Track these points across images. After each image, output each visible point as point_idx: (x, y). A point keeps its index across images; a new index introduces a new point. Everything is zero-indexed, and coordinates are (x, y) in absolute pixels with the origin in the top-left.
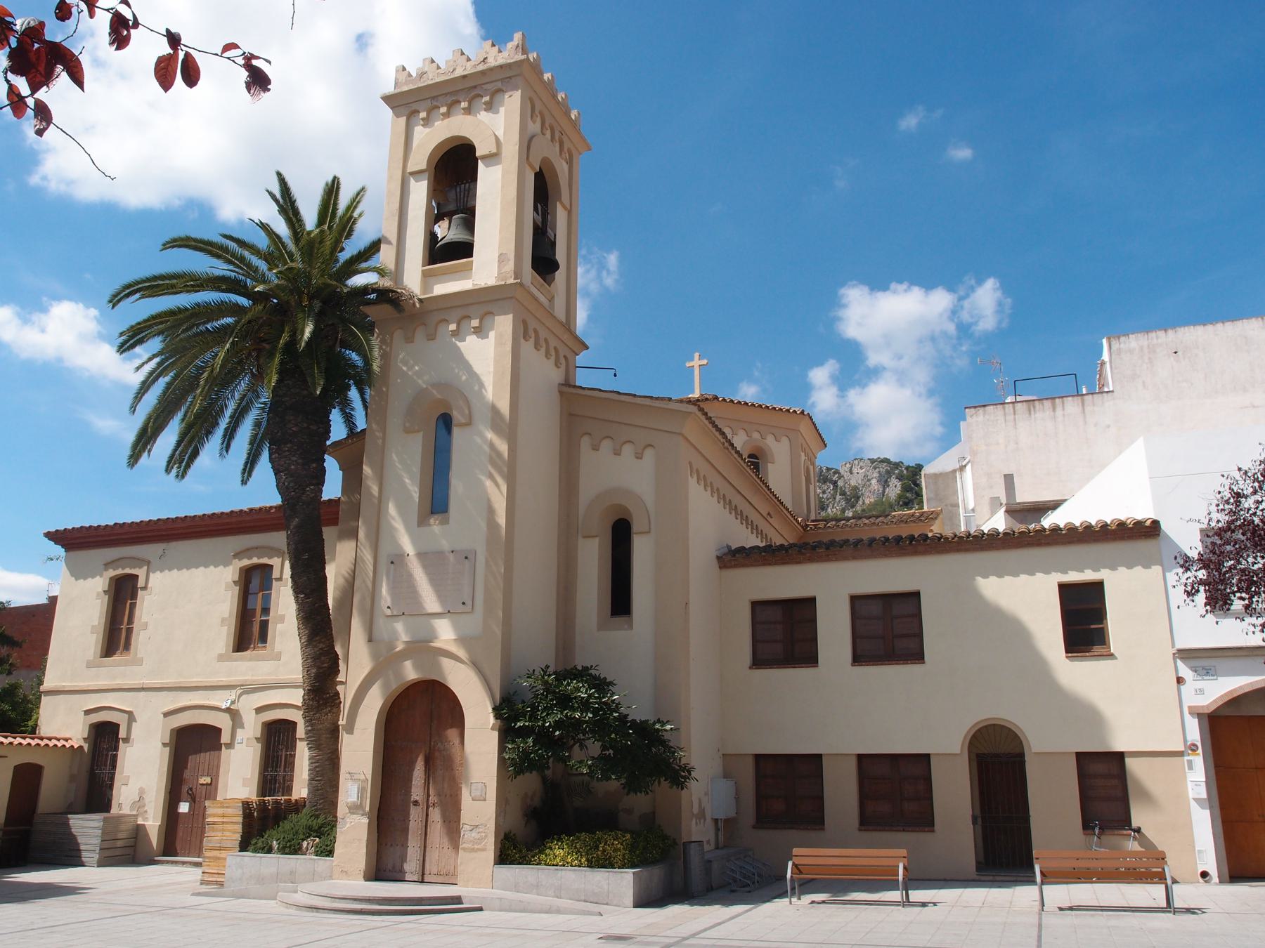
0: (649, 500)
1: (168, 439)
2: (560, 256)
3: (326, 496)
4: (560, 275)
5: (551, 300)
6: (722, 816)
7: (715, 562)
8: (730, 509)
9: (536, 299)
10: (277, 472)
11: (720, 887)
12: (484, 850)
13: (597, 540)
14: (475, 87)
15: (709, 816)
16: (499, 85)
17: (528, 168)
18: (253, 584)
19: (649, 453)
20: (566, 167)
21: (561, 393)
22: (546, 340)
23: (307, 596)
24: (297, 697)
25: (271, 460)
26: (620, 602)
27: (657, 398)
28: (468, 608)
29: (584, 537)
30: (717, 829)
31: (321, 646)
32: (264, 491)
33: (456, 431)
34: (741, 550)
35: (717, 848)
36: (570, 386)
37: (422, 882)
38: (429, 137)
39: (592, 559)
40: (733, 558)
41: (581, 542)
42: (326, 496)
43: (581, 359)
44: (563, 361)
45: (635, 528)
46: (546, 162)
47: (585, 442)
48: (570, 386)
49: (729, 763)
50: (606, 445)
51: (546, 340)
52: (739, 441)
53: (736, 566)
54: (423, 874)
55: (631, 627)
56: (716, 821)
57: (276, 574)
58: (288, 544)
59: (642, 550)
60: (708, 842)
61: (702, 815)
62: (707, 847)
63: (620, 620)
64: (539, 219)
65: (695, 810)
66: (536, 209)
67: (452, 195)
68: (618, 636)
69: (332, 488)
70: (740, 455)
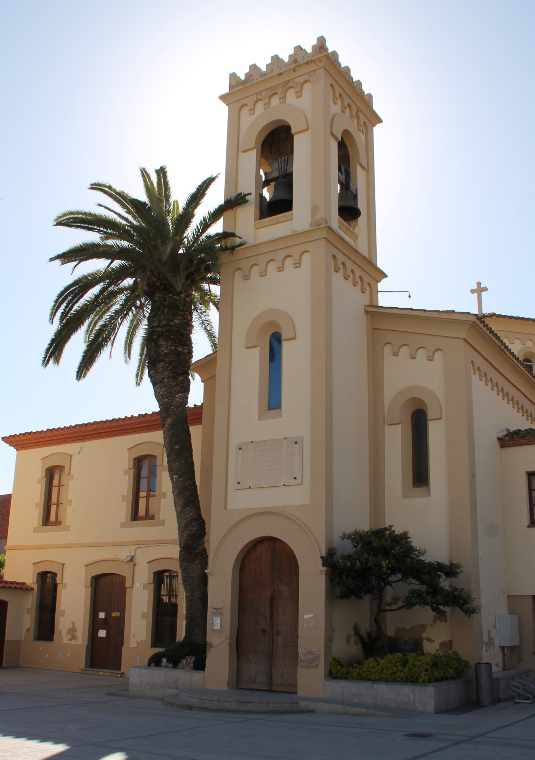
0: (440, 395)
1: (77, 344)
2: (361, 205)
3: (191, 404)
4: (362, 219)
5: (355, 237)
6: (507, 643)
7: (497, 443)
8: (509, 400)
9: (342, 239)
10: (154, 384)
11: (506, 700)
12: (316, 666)
13: (399, 426)
14: (288, 81)
15: (497, 642)
16: (306, 77)
17: (332, 140)
18: (141, 465)
19: (438, 354)
20: (363, 137)
21: (366, 312)
22: (343, 263)
23: (179, 477)
24: (175, 551)
25: (150, 376)
26: (420, 476)
27: (443, 312)
28: (298, 481)
29: (389, 425)
30: (504, 655)
31: (191, 514)
32: (144, 400)
33: (284, 344)
34: (517, 433)
35: (504, 669)
36: (373, 306)
37: (270, 691)
38: (258, 120)
39: (396, 442)
40: (512, 439)
41: (387, 428)
42: (191, 404)
43: (382, 285)
44: (358, 280)
45: (429, 416)
46: (346, 132)
47: (388, 349)
48: (373, 306)
49: (513, 601)
50: (404, 351)
51: (343, 263)
52: (516, 348)
53: (514, 445)
54: (271, 685)
55: (429, 494)
56: (503, 648)
57: (158, 462)
58: (165, 438)
59: (436, 432)
60: (497, 665)
61: (491, 643)
62: (494, 669)
63: (421, 490)
64: (343, 177)
65: (485, 639)
66: (340, 170)
67: (275, 165)
68: (419, 502)
69: (196, 396)
70: (517, 359)
